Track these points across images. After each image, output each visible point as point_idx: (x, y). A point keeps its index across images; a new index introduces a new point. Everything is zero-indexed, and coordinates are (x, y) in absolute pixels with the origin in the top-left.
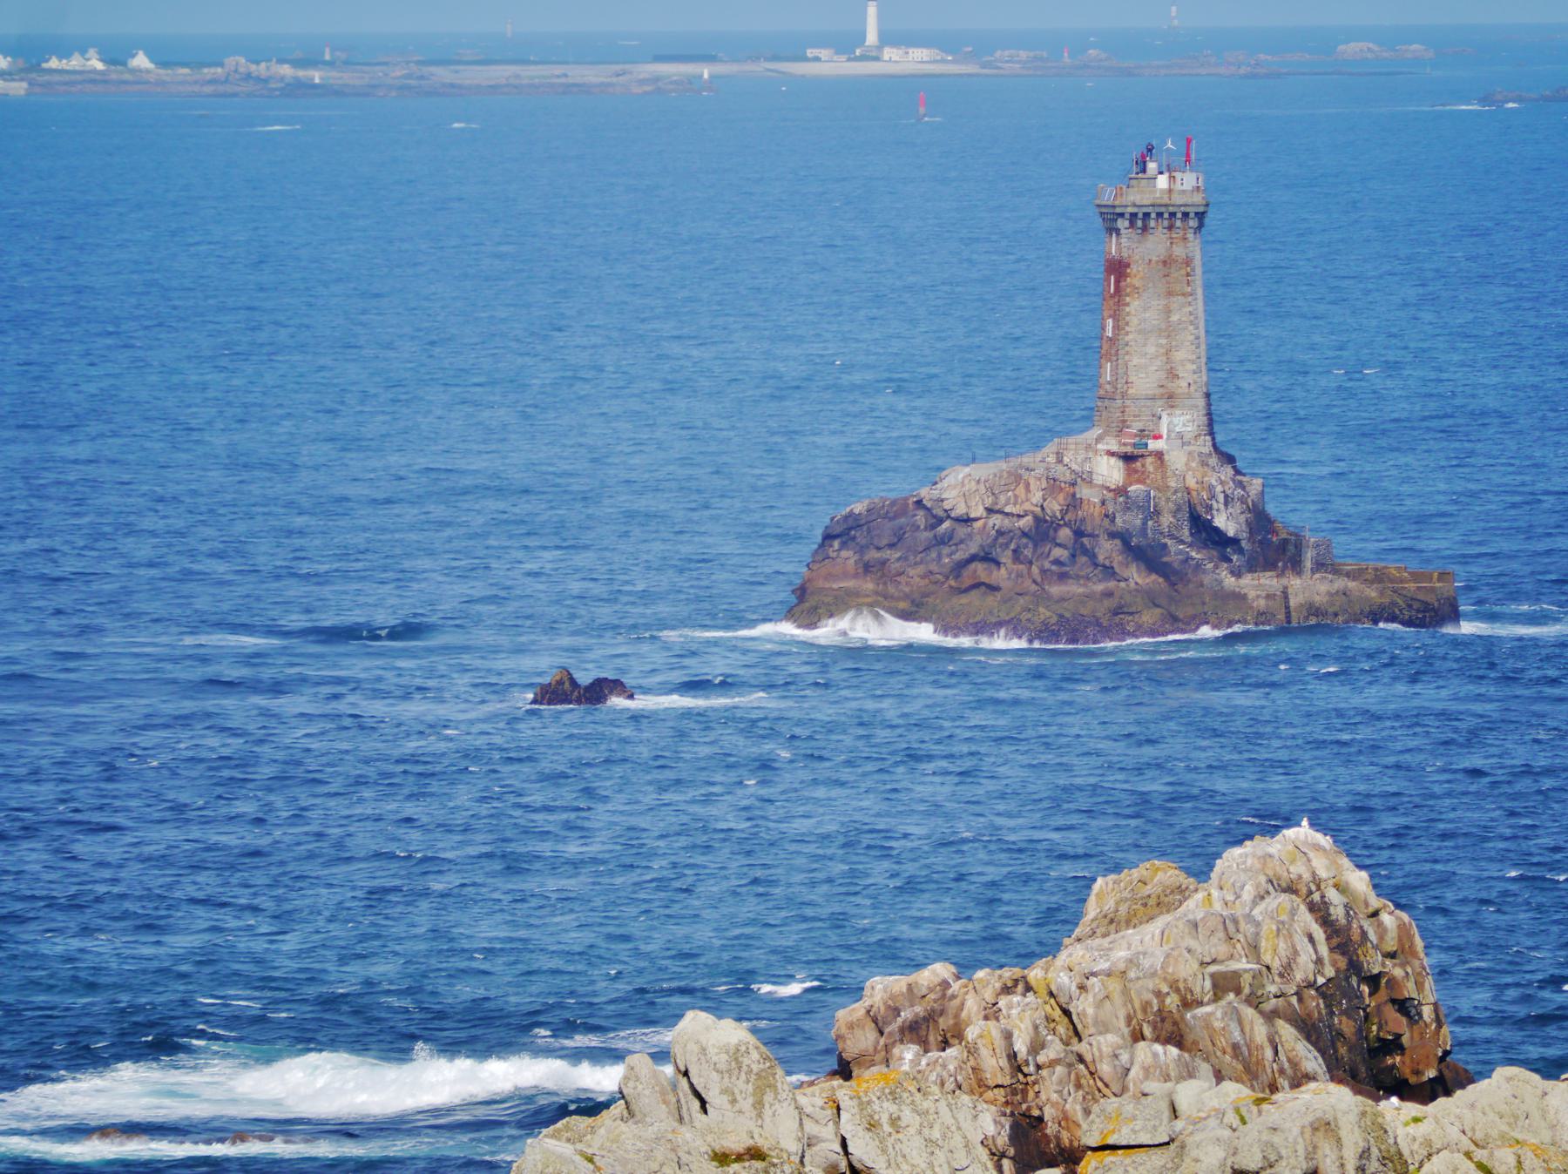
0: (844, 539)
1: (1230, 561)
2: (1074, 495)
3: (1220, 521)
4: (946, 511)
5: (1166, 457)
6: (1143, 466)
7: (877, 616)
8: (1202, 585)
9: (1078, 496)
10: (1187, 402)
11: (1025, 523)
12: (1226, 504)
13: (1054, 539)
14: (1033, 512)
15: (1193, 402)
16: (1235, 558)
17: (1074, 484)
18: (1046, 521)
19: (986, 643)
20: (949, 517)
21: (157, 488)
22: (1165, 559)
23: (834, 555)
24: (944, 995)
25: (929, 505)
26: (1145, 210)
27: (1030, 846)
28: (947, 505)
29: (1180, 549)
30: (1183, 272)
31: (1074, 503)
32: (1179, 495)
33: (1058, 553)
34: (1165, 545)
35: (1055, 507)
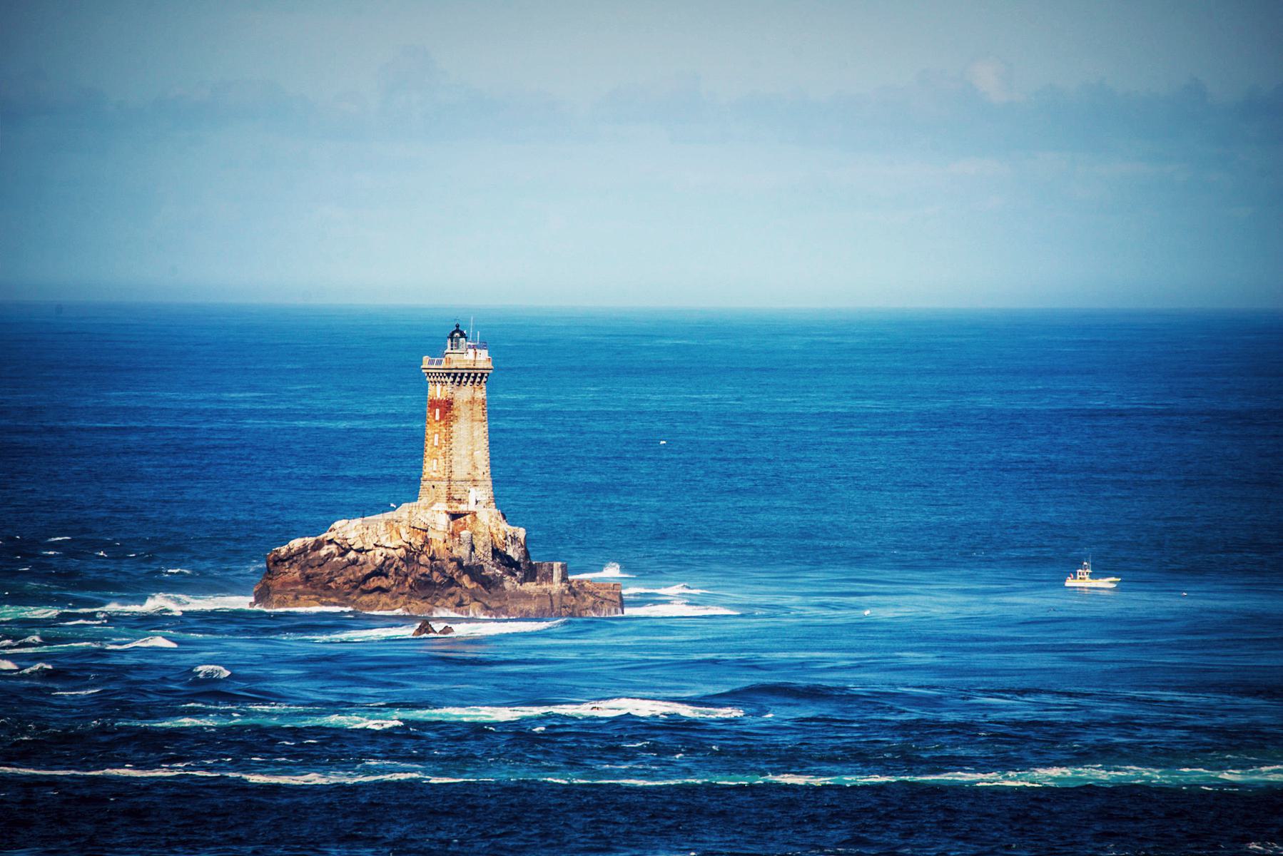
0: (291, 561)
1: (516, 575)
2: (426, 537)
3: (510, 552)
4: (350, 545)
5: (477, 515)
6: (465, 520)
7: (153, 597)
8: (505, 589)
9: (429, 537)
10: (482, 483)
11: (401, 552)
12: (512, 542)
13: (418, 562)
14: (404, 547)
15: (486, 483)
16: (518, 573)
17: (426, 531)
18: (411, 552)
19: (1153, 641)
20: (352, 549)
21: (944, 517)
22: (483, 574)
23: (287, 570)
24: (598, 805)
25: (338, 541)
26: (462, 371)
27: (1005, 763)
28: (350, 542)
29: (491, 569)
30: (480, 408)
31: (427, 542)
32: (486, 537)
33: (423, 570)
34: (482, 566)
35: (418, 541)
